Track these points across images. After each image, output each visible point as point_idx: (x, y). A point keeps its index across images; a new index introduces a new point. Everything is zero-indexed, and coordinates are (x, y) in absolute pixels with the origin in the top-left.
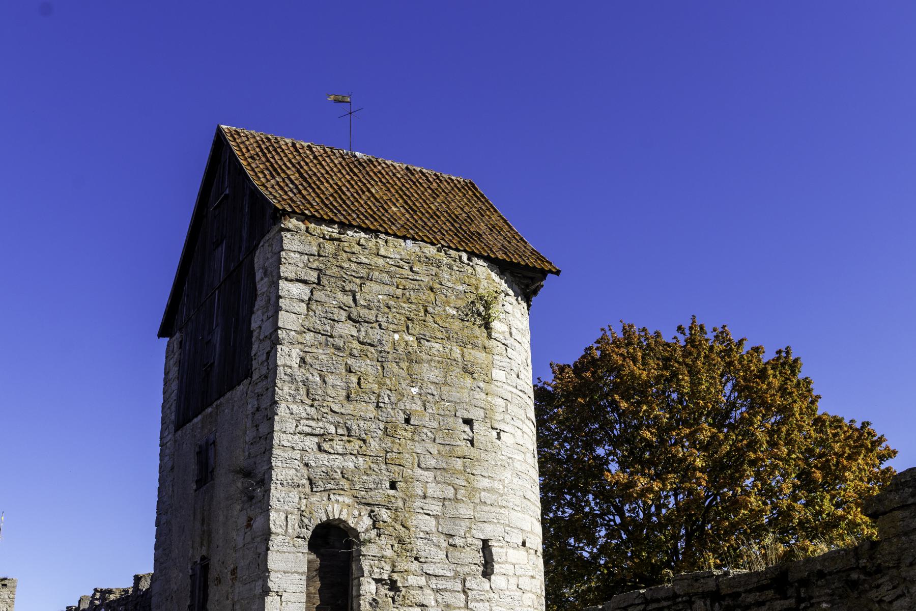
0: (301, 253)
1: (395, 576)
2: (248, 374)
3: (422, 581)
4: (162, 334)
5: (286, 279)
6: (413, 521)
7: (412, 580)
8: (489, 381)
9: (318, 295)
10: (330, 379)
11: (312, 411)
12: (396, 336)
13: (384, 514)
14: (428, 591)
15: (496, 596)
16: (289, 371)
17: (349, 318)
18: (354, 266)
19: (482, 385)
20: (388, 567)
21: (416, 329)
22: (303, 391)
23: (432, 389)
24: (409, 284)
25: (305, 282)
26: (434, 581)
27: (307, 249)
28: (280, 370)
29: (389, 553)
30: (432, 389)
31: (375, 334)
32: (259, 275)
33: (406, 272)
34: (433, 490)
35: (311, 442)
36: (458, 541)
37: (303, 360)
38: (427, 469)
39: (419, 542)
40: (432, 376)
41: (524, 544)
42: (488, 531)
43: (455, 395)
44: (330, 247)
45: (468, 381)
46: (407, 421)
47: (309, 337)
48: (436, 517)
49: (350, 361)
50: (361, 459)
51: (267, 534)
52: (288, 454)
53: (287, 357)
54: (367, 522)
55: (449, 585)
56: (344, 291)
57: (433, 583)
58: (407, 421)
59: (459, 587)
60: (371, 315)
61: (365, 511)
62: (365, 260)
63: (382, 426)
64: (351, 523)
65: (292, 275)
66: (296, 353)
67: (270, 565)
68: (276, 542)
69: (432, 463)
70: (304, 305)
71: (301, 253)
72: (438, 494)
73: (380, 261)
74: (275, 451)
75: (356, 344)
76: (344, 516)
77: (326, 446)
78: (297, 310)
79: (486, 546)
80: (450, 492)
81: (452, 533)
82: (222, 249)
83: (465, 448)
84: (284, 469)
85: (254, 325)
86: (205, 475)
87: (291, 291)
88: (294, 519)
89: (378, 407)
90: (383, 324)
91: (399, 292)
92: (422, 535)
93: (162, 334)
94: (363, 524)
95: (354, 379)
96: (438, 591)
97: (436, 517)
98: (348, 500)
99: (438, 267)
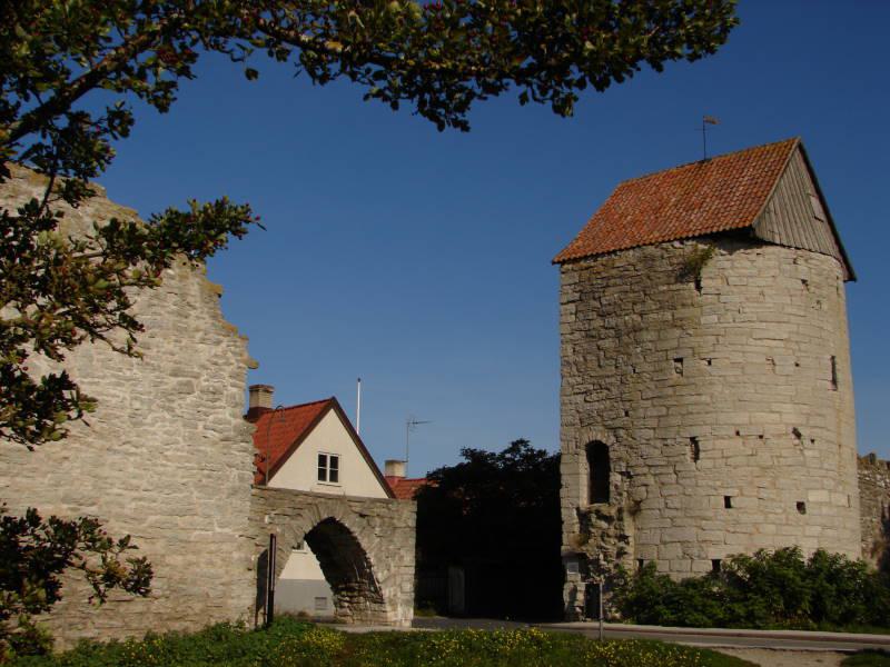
0: (570, 285)
1: (629, 470)
3: (646, 470)
6: (638, 433)
10: (589, 357)
12: (627, 318)
14: (649, 476)
15: (702, 474)
18: (599, 281)
20: (624, 464)
22: (574, 369)
23: (650, 345)
26: (653, 469)
27: (571, 281)
30: (650, 345)
35: (580, 399)
36: (669, 442)
38: (647, 399)
39: (642, 446)
40: (649, 337)
41: (738, 433)
42: (695, 432)
44: (586, 274)
47: (577, 335)
48: (654, 429)
50: (608, 402)
51: (355, 538)
54: (613, 439)
55: (663, 470)
56: (594, 299)
59: (671, 471)
63: (619, 378)
64: (604, 441)
67: (562, 472)
69: (650, 395)
70: (573, 316)
71: (570, 285)
72: (655, 414)
76: (599, 438)
77: (588, 399)
79: (693, 440)
80: (664, 411)
81: (365, 512)
89: (617, 367)
92: (644, 441)
96: (655, 475)
97: (654, 429)
98: (601, 428)
99: (653, 260)
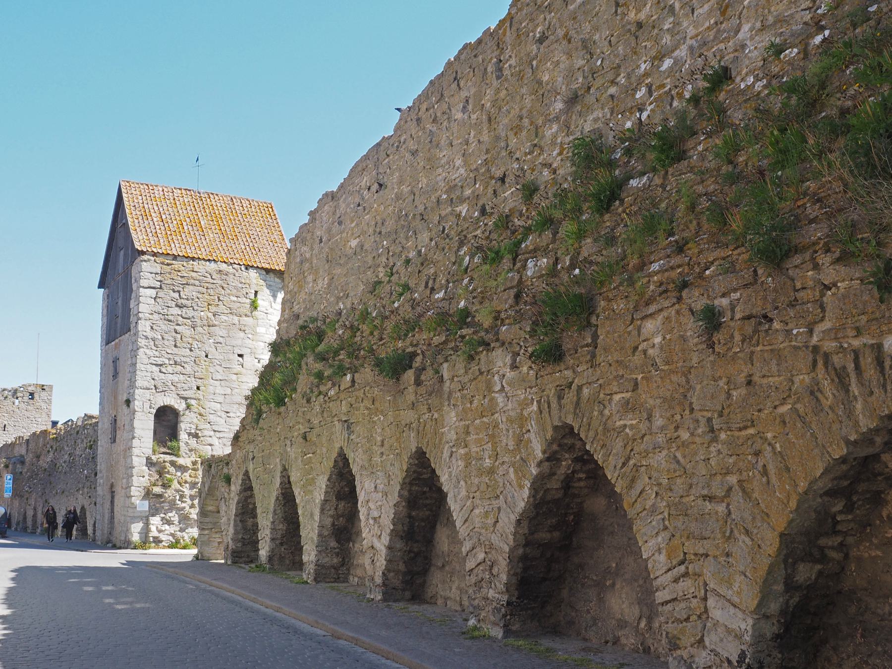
2: (129, 330)
3: (212, 433)
4: (99, 287)
5: (143, 287)
6: (208, 405)
7: (206, 433)
8: (255, 333)
9: (161, 294)
11: (157, 354)
12: (202, 313)
13: (193, 402)
14: (214, 438)
16: (145, 334)
17: (177, 306)
19: (250, 336)
20: (194, 427)
21: (213, 309)
24: (210, 286)
25: (154, 288)
28: (140, 333)
29: (195, 420)
31: (190, 313)
32: (133, 281)
33: (209, 280)
34: (220, 390)
36: (231, 415)
37: (152, 328)
43: (234, 343)
45: (242, 334)
46: (207, 356)
47: (156, 316)
49: (177, 327)
52: (145, 373)
53: (144, 327)
56: (174, 292)
57: (218, 435)
58: (207, 356)
60: (189, 303)
61: (183, 402)
62: (185, 275)
64: (176, 406)
65: (146, 285)
66: (148, 323)
68: (138, 415)
73: (194, 274)
74: (137, 372)
75: (180, 318)
76: (172, 403)
77: (164, 370)
78: (149, 302)
82: (122, 252)
83: (238, 368)
84: (142, 380)
85: (132, 306)
86: (115, 375)
87: (146, 295)
88: (147, 405)
90: (196, 308)
91: (204, 290)
93: (99, 287)
94: (180, 406)
95: (179, 336)
